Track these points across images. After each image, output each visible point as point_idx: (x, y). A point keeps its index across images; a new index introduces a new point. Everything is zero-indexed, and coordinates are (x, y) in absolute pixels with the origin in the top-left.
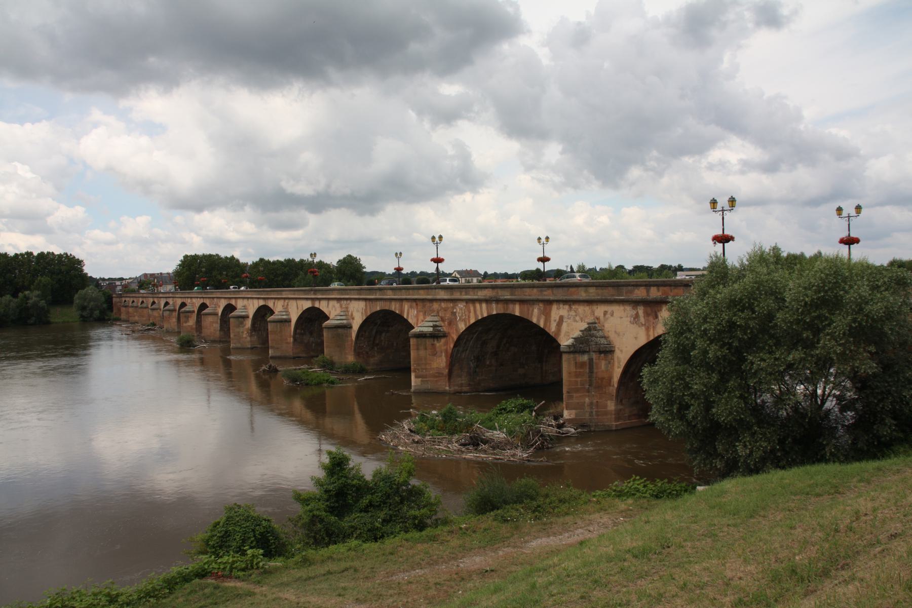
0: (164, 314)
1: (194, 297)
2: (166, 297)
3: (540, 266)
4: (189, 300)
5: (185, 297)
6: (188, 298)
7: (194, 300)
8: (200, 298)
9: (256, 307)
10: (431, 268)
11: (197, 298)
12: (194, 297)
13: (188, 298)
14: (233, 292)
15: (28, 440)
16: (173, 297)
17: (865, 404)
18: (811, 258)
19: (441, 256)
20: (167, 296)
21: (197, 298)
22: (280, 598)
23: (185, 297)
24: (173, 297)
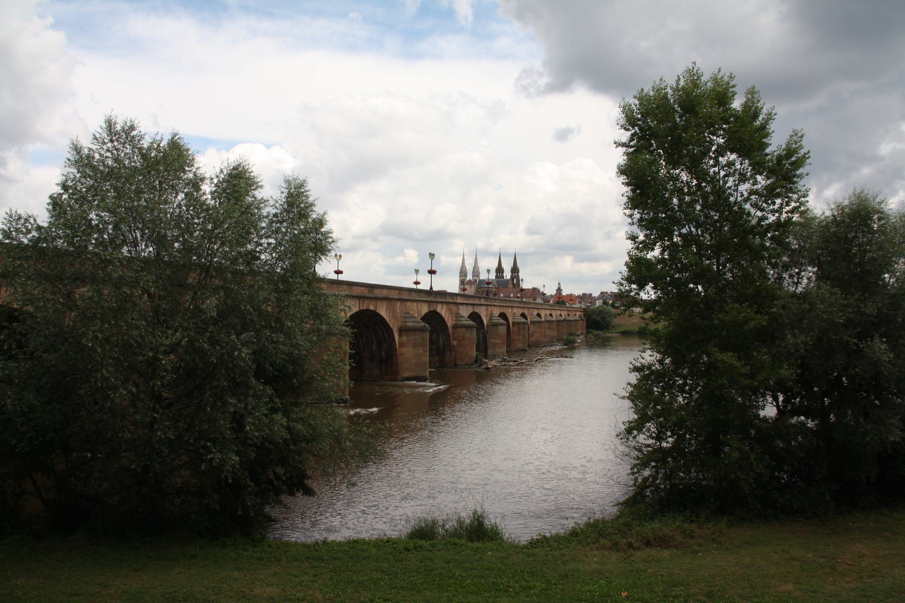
0: (500, 327)
1: (515, 307)
2: (473, 305)
3: (414, 287)
4: (510, 310)
5: (505, 306)
6: (508, 307)
7: (515, 310)
8: (521, 307)
9: (355, 310)
10: (334, 277)
11: (518, 307)
12: (515, 307)
13: (508, 307)
14: (503, 300)
15: (720, 69)
16: (487, 305)
17: (105, 337)
18: (434, 291)
19: (419, 280)
20: (476, 302)
21: (518, 307)
22: (600, 564)
23: (505, 306)
24: (487, 305)
